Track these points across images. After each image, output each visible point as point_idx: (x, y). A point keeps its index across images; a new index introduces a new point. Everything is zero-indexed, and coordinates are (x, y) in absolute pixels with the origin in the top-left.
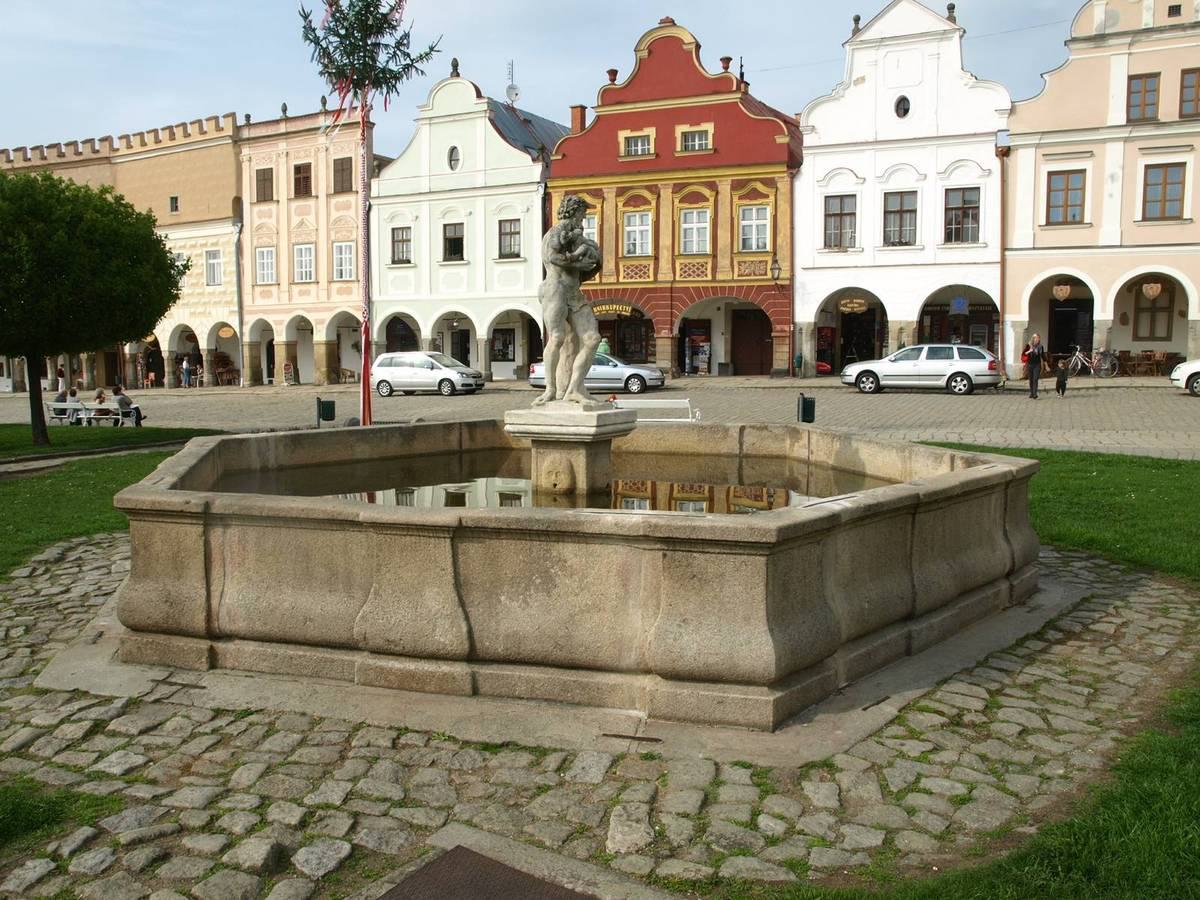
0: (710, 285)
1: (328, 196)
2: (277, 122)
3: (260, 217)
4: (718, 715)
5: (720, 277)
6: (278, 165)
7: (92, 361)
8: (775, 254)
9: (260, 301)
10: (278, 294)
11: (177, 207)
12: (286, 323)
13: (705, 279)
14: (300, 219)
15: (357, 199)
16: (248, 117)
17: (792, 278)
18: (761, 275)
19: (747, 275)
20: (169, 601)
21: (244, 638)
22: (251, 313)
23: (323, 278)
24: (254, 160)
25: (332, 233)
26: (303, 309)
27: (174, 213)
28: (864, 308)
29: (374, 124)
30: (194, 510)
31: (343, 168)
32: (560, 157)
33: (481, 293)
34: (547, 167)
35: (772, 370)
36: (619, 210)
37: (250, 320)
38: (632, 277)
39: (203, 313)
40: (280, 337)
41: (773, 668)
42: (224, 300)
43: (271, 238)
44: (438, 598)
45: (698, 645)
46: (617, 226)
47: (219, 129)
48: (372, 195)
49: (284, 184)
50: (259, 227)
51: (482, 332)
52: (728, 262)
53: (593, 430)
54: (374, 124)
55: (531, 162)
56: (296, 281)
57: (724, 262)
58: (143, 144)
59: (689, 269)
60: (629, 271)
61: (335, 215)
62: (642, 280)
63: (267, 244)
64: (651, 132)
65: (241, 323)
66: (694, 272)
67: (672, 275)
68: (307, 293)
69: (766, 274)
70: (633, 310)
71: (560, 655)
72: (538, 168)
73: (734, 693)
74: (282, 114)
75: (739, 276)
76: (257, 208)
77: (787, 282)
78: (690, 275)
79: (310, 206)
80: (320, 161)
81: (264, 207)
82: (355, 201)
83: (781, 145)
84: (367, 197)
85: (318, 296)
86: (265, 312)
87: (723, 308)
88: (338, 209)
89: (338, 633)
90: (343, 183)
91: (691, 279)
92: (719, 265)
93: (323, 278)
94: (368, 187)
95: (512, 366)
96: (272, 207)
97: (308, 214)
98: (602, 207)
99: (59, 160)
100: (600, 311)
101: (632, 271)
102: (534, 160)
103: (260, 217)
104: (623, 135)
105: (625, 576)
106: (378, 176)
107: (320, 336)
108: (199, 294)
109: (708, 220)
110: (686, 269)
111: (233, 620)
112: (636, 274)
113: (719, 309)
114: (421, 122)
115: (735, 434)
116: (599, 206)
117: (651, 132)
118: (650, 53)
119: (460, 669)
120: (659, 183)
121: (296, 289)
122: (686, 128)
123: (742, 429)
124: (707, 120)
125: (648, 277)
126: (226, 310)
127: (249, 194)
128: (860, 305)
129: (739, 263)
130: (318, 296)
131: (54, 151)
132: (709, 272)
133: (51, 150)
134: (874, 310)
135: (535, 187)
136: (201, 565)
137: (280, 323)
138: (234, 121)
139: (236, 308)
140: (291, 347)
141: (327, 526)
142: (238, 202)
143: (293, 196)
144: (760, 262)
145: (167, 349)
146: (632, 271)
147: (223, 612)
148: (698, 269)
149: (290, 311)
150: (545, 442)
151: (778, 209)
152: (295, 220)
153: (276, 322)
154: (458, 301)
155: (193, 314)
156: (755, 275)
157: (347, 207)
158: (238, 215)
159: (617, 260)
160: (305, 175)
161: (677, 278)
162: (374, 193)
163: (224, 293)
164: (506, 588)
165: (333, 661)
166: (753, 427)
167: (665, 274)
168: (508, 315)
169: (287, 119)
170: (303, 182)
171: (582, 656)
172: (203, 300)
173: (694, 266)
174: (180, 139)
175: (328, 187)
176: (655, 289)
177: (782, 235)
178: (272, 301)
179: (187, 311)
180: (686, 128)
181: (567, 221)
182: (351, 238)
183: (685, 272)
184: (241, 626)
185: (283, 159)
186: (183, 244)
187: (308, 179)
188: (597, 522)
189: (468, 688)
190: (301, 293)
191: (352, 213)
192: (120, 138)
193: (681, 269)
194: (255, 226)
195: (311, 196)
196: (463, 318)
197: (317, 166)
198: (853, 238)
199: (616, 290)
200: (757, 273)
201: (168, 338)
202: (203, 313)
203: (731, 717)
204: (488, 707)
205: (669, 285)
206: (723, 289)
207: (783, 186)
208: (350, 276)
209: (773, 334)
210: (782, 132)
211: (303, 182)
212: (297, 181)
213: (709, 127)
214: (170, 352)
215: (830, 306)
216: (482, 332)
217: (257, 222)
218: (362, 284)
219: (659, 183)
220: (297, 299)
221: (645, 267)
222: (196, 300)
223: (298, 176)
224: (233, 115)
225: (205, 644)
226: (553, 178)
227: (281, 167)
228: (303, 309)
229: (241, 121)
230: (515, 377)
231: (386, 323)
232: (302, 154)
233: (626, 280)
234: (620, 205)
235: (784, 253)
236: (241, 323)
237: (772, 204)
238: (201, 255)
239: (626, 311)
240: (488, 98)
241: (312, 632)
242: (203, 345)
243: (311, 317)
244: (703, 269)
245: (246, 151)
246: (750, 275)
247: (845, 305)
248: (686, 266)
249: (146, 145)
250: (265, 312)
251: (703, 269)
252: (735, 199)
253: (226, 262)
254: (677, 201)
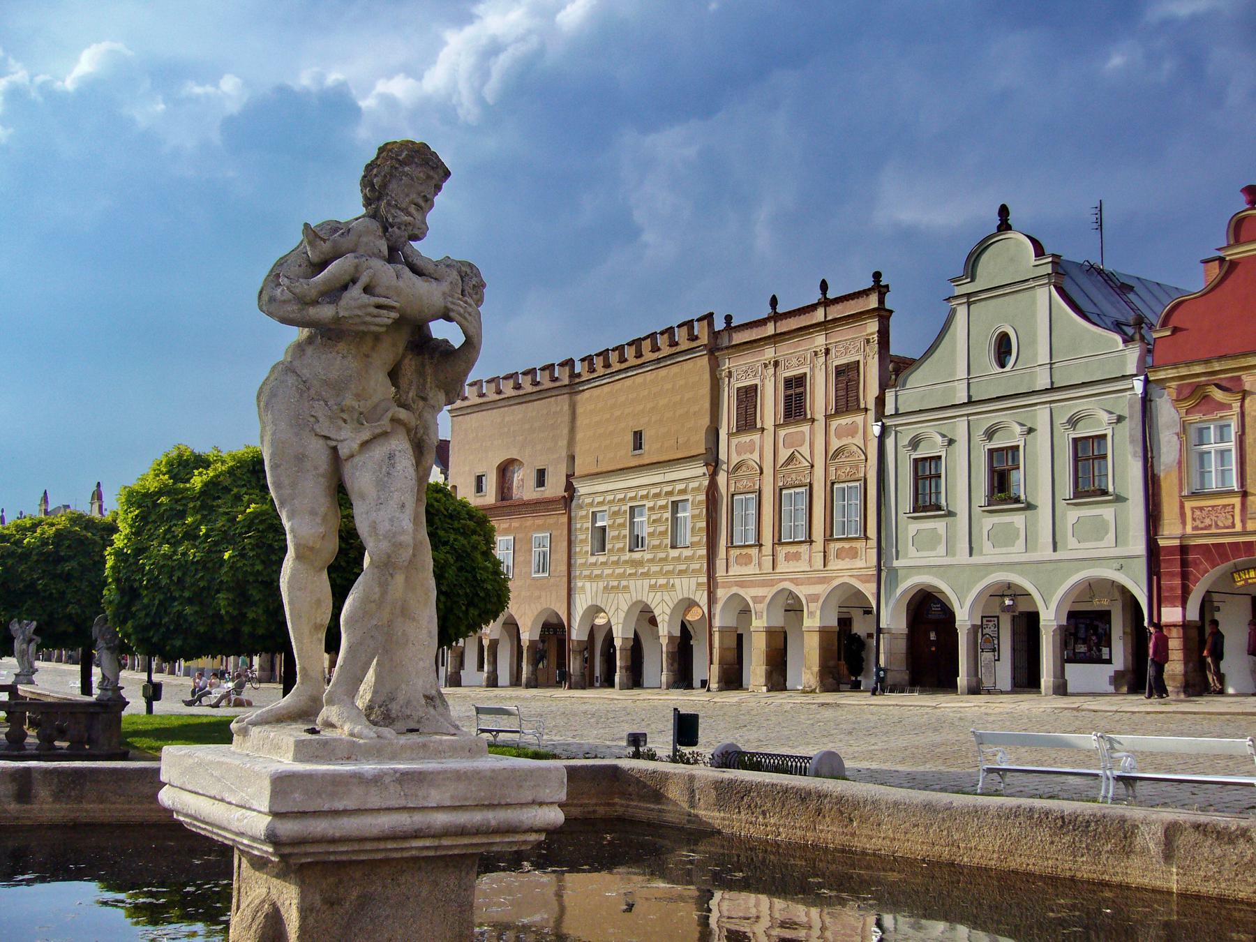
1: (730, 435)
2: (811, 308)
6: (812, 369)
8: (1244, 494)
11: (641, 444)
15: (812, 432)
16: (728, 319)
18: (1227, 528)
22: (727, 585)
24: (833, 352)
25: (832, 469)
26: (791, 580)
27: (637, 452)
29: (891, 312)
31: (847, 376)
32: (1168, 333)
33: (1046, 553)
42: (640, 571)
43: (857, 467)
47: (693, 338)
48: (887, 413)
49: (770, 407)
50: (738, 466)
51: (1050, 619)
54: (891, 312)
55: (1121, 346)
58: (673, 344)
61: (835, 444)
65: (712, 599)
68: (797, 557)
69: (1233, 526)
74: (820, 296)
81: (745, 438)
85: (759, 564)
86: (741, 584)
90: (847, 401)
94: (880, 401)
95: (1107, 671)
99: (674, 350)
103: (739, 453)
108: (661, 560)
109: (1233, 438)
114: (954, 302)
116: (1237, 406)
126: (693, 581)
130: (759, 564)
131: (511, 383)
133: (525, 377)
138: (711, 325)
139: (704, 579)
141: (387, 811)
144: (1225, 506)
145: (620, 635)
152: (784, 454)
153: (755, 599)
154: (1011, 566)
155: (653, 588)
169: (826, 303)
172: (666, 568)
174: (648, 355)
182: (857, 476)
185: (771, 370)
186: (645, 492)
187: (801, 396)
190: (788, 557)
192: (583, 360)
195: (805, 419)
196: (1011, 591)
197: (812, 377)
200: (1220, 524)
201: (529, 624)
208: (856, 533)
212: (788, 398)
216: (1050, 619)
218: (873, 543)
220: (782, 566)
223: (789, 392)
224: (709, 317)
226: (1155, 368)
227: (817, 371)
228: (791, 580)
229: (719, 325)
230: (1111, 689)
236: (712, 599)
240: (1053, 255)
243: (802, 592)
245: (729, 364)
249: (677, 344)
253: (692, 516)
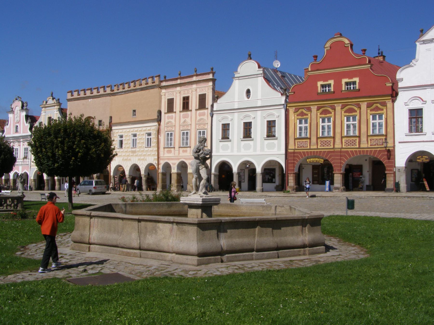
0: (358, 150)
3: (168, 119)
4: (186, 262)
5: (362, 146)
7: (98, 177)
9: (167, 155)
10: (174, 152)
12: (177, 164)
13: (355, 147)
14: (184, 119)
17: (394, 147)
18: (380, 145)
19: (374, 145)
20: (82, 235)
21: (96, 244)
23: (177, 147)
25: (197, 126)
26: (184, 158)
27: (134, 116)
28: (428, 160)
30: (88, 214)
31: (202, 98)
34: (287, 97)
35: (386, 189)
36: (318, 116)
37: (162, 162)
38: (323, 146)
39: (143, 159)
40: (174, 170)
41: (197, 251)
44: (135, 235)
45: (183, 246)
46: (317, 123)
49: (178, 105)
50: (168, 123)
52: (366, 139)
53: (201, 203)
56: (181, 146)
57: (364, 139)
59: (349, 142)
60: (322, 143)
61: (198, 118)
62: (328, 147)
63: (170, 130)
64: (332, 82)
66: (351, 144)
67: (341, 145)
68: (186, 151)
70: (324, 161)
71: (157, 248)
72: (284, 98)
73: (190, 257)
75: (371, 145)
76: (167, 115)
77: (392, 148)
78: (349, 145)
79: (188, 114)
80: (193, 95)
81: (170, 115)
82: (207, 112)
83: (389, 87)
84: (212, 110)
86: (168, 159)
87: (368, 160)
88: (200, 115)
89: (114, 243)
90: (202, 105)
91: (349, 147)
92: (362, 141)
93: (177, 147)
94: (212, 106)
96: (173, 114)
97: (188, 117)
98: (311, 115)
100: (310, 161)
101: (324, 143)
102: (282, 94)
103: (168, 119)
104: (319, 83)
105: (171, 230)
106: (217, 102)
107: (174, 170)
108: (142, 151)
110: (347, 142)
111: (94, 240)
112: (325, 144)
113: (366, 160)
115: (273, 208)
117: (332, 82)
118: (330, 48)
119: (138, 251)
120: (335, 105)
121: (181, 150)
122: (347, 80)
123: (276, 207)
124: (356, 76)
125: (331, 146)
127: (164, 108)
128: (426, 159)
129: (371, 140)
132: (357, 144)
134: (274, 170)
135: (282, 107)
136: (89, 227)
137: (174, 164)
140: (179, 175)
142: (160, 112)
143: (181, 110)
144: (380, 139)
146: (324, 143)
147: (92, 238)
148: (352, 142)
149: (178, 159)
150: (192, 206)
151: (388, 116)
152: (182, 120)
155: (139, 159)
156: (378, 145)
157: (204, 114)
158: (159, 120)
159: (317, 138)
160: (185, 101)
161: (343, 147)
162: (215, 109)
163: (152, 151)
164: (148, 233)
165: (113, 250)
166: (279, 206)
167: (338, 145)
168: (270, 162)
170: (186, 106)
171: (162, 249)
173: (351, 141)
175: (196, 106)
176: (334, 152)
177: (389, 127)
178: (171, 155)
179: (137, 158)
180: (347, 80)
181: (200, 144)
183: (347, 144)
184: (96, 241)
188: (230, 237)
189: (139, 256)
190: (184, 151)
191: (205, 117)
193: (345, 142)
194: (166, 122)
196: (251, 163)
197: (192, 97)
198: (422, 128)
199: (320, 152)
200: (379, 144)
202: (143, 159)
203: (189, 263)
204: (142, 259)
205: (340, 150)
206: (363, 151)
207: (389, 104)
209: (386, 172)
210: (389, 81)
211: (186, 106)
212: (184, 104)
213: (357, 80)
214: (129, 175)
215: (412, 159)
217: (167, 121)
219: (335, 105)
221: (329, 141)
222: (141, 154)
223: (185, 101)
225: (88, 246)
226: (290, 103)
228: (184, 158)
231: (218, 166)
232: (186, 92)
233: (321, 147)
234: (319, 114)
235: (390, 136)
236: (158, 164)
237: (385, 113)
238: (143, 134)
239: (322, 161)
241: (110, 243)
242: (143, 172)
244: (355, 142)
246: (375, 145)
247: (419, 159)
248: (347, 141)
250: (168, 159)
251: (355, 142)
252: (369, 111)
254: (343, 112)
